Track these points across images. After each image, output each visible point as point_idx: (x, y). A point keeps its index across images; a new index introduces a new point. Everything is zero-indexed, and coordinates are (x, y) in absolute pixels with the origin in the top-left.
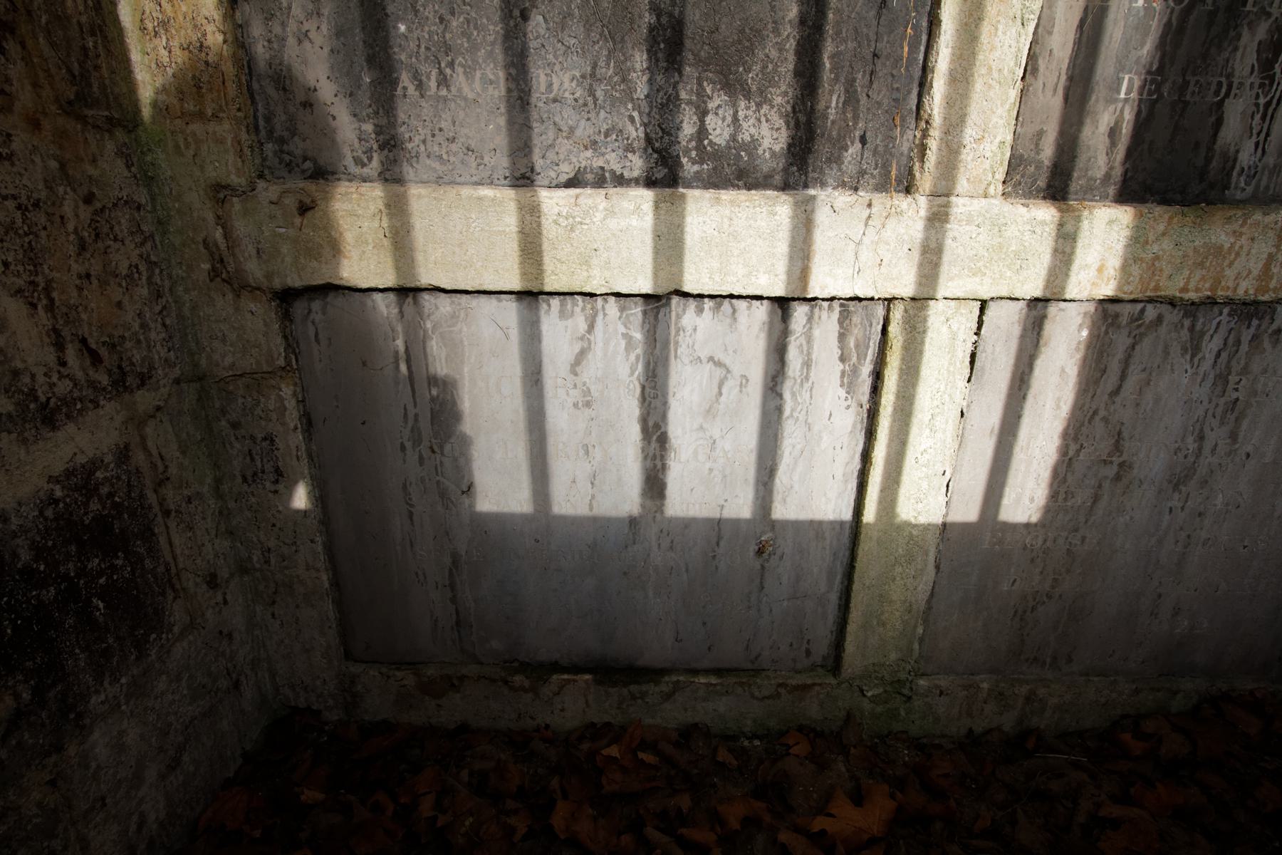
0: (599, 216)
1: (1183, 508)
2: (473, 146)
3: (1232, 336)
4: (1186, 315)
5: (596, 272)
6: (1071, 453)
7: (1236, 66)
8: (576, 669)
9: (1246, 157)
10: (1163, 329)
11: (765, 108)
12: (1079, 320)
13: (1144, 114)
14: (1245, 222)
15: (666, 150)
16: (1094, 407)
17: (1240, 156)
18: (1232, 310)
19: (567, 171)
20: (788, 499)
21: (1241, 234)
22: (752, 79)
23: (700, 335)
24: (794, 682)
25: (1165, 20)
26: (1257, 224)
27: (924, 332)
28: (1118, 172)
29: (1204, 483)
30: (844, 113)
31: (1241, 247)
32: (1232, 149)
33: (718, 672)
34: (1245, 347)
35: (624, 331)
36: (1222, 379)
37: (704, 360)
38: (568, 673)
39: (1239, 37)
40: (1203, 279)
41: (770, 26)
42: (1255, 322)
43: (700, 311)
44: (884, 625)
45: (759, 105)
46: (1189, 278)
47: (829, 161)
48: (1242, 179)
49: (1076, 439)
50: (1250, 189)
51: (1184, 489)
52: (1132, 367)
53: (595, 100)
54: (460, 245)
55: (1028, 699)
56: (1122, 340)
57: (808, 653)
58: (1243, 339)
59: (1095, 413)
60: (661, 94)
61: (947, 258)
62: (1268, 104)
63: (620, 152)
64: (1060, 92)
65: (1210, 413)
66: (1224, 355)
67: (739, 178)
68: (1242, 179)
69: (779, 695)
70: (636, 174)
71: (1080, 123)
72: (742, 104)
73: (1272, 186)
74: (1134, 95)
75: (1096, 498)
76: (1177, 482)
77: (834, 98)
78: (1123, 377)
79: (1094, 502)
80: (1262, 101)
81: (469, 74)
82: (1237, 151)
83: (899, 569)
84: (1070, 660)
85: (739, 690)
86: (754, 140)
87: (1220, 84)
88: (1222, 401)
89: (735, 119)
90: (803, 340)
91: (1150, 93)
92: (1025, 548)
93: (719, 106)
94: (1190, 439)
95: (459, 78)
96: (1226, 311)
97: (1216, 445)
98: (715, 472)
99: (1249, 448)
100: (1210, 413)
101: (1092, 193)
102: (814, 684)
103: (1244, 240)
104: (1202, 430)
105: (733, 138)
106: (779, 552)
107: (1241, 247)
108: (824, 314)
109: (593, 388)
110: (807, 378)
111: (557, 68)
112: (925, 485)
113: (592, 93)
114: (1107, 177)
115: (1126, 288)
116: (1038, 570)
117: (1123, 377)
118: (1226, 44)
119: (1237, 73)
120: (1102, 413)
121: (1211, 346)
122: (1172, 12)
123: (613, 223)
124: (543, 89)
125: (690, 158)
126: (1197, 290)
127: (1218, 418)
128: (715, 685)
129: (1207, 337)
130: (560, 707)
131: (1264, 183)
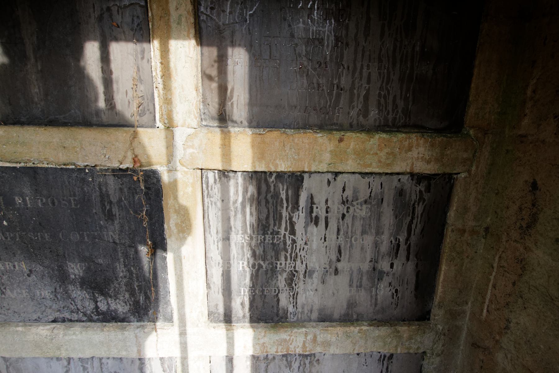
0: (61, 336)
2: (16, 311)
5: (63, 352)
9: (291, 309)
11: (118, 301)
13: (251, 298)
14: (292, 332)
17: (289, 309)
19: (51, 318)
22: (111, 292)
23: (110, 365)
27: (188, 366)
28: (248, 315)
32: (286, 308)
34: (308, 365)
39: (277, 277)
40: (282, 348)
45: (115, 300)
47: (144, 314)
48: (292, 315)
50: (295, 318)
53: (58, 298)
54: (12, 345)
62: (294, 295)
66: (301, 368)
68: (292, 315)
71: (230, 302)
72: (110, 299)
74: (247, 293)
77: (141, 297)
80: (291, 294)
81: (12, 291)
86: (115, 309)
87: (275, 290)
89: (108, 303)
91: (251, 293)
95: (8, 292)
103: (293, 337)
105: (108, 308)
111: (43, 289)
113: (56, 296)
114: (244, 316)
119: (280, 286)
123: (66, 338)
124: (39, 295)
126: (281, 352)
129: (293, 363)
131: (300, 316)
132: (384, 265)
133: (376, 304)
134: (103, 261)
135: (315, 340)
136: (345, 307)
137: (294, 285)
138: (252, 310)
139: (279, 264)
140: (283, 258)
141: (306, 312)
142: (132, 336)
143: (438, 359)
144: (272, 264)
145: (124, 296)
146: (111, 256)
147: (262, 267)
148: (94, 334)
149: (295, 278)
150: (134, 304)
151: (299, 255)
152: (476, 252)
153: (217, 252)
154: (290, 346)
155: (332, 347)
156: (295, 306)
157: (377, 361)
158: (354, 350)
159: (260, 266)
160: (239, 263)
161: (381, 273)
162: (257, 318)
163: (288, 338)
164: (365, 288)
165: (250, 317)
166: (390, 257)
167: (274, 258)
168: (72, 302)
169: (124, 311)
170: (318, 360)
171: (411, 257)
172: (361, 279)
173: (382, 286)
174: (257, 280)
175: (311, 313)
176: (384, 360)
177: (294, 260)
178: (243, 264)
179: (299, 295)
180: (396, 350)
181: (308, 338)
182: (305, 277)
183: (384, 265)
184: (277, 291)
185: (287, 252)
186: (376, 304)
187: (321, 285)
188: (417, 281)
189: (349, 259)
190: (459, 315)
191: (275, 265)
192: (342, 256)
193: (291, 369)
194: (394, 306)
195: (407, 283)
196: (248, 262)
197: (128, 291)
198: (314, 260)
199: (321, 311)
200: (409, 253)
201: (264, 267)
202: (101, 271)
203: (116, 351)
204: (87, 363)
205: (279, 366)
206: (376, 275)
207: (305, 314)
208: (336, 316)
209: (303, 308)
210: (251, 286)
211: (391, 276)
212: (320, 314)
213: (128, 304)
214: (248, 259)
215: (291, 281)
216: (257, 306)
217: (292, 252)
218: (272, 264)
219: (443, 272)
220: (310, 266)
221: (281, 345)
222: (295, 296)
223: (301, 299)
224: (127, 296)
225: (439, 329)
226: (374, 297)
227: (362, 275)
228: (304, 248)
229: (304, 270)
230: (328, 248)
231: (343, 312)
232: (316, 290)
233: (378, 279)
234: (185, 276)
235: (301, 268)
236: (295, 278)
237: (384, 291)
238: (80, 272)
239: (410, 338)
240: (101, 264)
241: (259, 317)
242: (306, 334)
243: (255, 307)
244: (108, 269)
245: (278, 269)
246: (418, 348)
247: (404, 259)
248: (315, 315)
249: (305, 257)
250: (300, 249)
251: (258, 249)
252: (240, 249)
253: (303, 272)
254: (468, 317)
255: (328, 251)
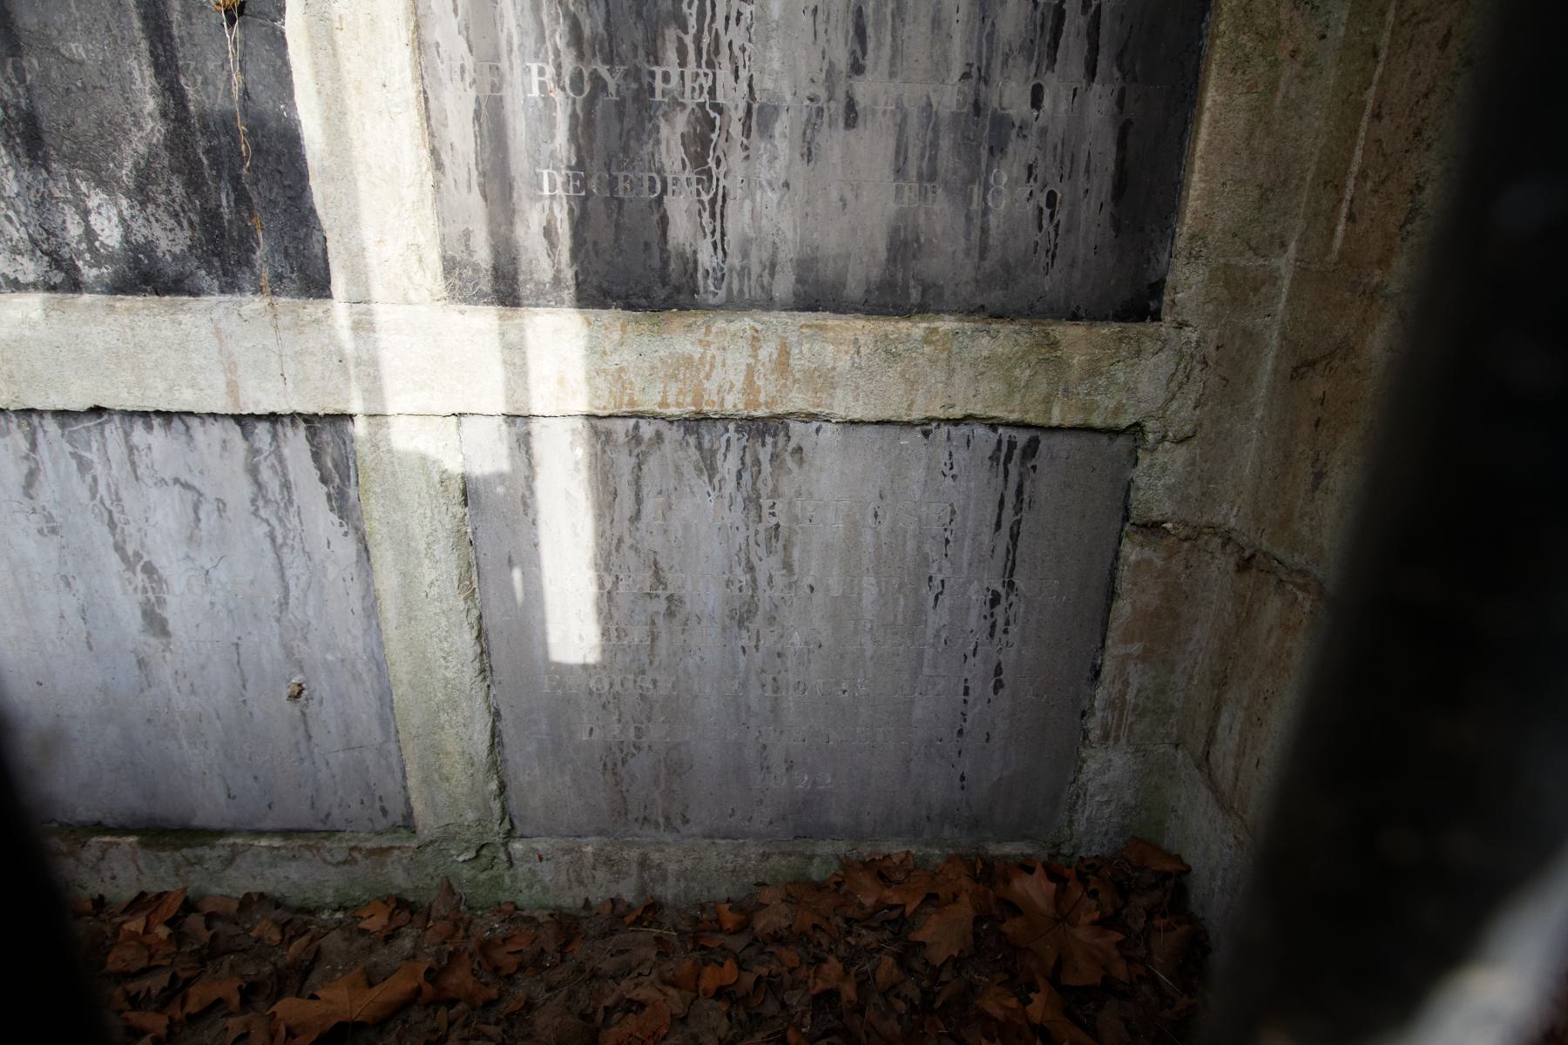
1: (756, 647)
3: (748, 455)
4: (687, 431)
6: (608, 586)
7: (664, 160)
8: (123, 831)
9: (706, 258)
10: (667, 447)
11: (151, 208)
12: (568, 437)
13: (577, 212)
15: (56, 252)
16: (617, 535)
17: (699, 256)
18: (738, 426)
20: (310, 637)
21: (708, 344)
23: (157, 454)
24: (369, 845)
25: (569, 110)
26: (723, 332)
28: (568, 274)
29: (772, 619)
30: (238, 212)
31: (713, 357)
32: (689, 251)
33: (287, 833)
34: (766, 468)
35: (71, 449)
36: (753, 501)
37: (171, 482)
38: (112, 835)
39: (657, 129)
40: (681, 392)
41: (129, 119)
42: (769, 440)
43: (150, 428)
44: (447, 779)
46: (665, 392)
48: (710, 281)
49: (608, 569)
50: (722, 293)
51: (751, 626)
52: (645, 491)
55: (644, 863)
56: (625, 462)
57: (384, 812)
58: (761, 457)
59: (620, 541)
60: (33, 192)
61: (386, 370)
62: (713, 201)
63: (7, 254)
64: (476, 189)
65: (752, 541)
66: (746, 476)
67: (146, 282)
68: (710, 281)
69: (354, 861)
70: (31, 278)
73: (746, 289)
74: (559, 191)
75: (654, 638)
76: (742, 616)
77: (223, 196)
78: (639, 500)
79: (653, 641)
80: (706, 198)
82: (695, 252)
83: (444, 717)
84: (686, 821)
85: (308, 854)
86: (149, 242)
87: (652, 179)
88: (761, 527)
90: (272, 459)
91: (577, 190)
92: (591, 693)
93: (100, 206)
94: (739, 571)
96: (732, 426)
97: (771, 577)
98: (218, 607)
99: (810, 580)
100: (752, 541)
101: (540, 298)
102: (392, 848)
103: (713, 350)
104: (748, 559)
106: (316, 695)
107: (713, 357)
108: (289, 431)
109: (54, 513)
110: (290, 501)
112: (444, 622)
114: (557, 281)
115: (597, 403)
116: (615, 718)
117: (639, 500)
118: (645, 137)
119: (667, 168)
120: (628, 541)
121: (728, 466)
122: (574, 102)
125: (86, 262)
126: (678, 405)
127: (763, 546)
128: (278, 848)
129: (720, 456)
130: (109, 874)
131: (735, 286)
132: (1011, 95)
133: (984, 250)
134: (87, 51)
135: (783, 364)
136: (882, 254)
137: (711, 163)
138: (581, 256)
139: (659, 77)
140: (672, 55)
141: (756, 269)
142: (203, 331)
143: (1182, 452)
144: (637, 79)
145: (168, 192)
146: (108, 29)
147: (605, 86)
148: (86, 322)
149: (714, 136)
150: (203, 223)
151: (724, 40)
152: (1323, 37)
153: (453, 23)
154: (707, 385)
155: (840, 393)
156: (719, 246)
157: (988, 463)
158: (910, 406)
159: (598, 84)
160: (527, 71)
161: (1001, 124)
162: (599, 287)
163: (697, 352)
164: (946, 183)
165: (578, 285)
166: (1030, 60)
167: (641, 52)
168: (11, 213)
169: (177, 250)
170: (799, 449)
171: (1103, 63)
172: (934, 145)
173: (1005, 179)
174: (591, 139)
175: (772, 275)
176: (1008, 458)
177: (710, 64)
178: (541, 72)
179: (730, 203)
180: (1048, 411)
181: (763, 354)
182: (747, 132)
183: (1011, 95)
184: (659, 186)
185: (686, 32)
186: (984, 250)
187: (800, 166)
188: (1121, 163)
189: (892, 63)
190: (1256, 290)
191: (646, 80)
192: (870, 54)
193: (716, 481)
194: (1044, 259)
195: (1087, 171)
196: (559, 67)
197: (178, 171)
198: (776, 65)
199: (806, 266)
200: (1094, 49)
201: (612, 88)
202: (84, 89)
203: (161, 386)
204: (88, 446)
205: (677, 468)
206: (983, 131)
207: (754, 277)
208: (854, 290)
209: (745, 255)
210: (573, 162)
211: (1033, 139)
212: (800, 280)
213: (185, 224)
214: (557, 53)
215: (700, 145)
216: (595, 243)
217: (700, 31)
218: (637, 79)
219: (1206, 117)
220: (765, 84)
221: (674, 377)
222: (717, 208)
223: (738, 220)
224: (178, 190)
225: (1188, 343)
226: (977, 222)
227: (936, 130)
228: (739, 14)
229: (742, 105)
230: (821, 16)
231: (875, 274)
232: (787, 185)
233: (991, 149)
234: (353, 102)
235: (732, 96)
236: (714, 136)
237: (1009, 197)
238: (17, 96)
239: (1093, 371)
240: (81, 63)
241: (605, 285)
242: (755, 341)
243: (589, 246)
244: (104, 82)
245: (658, 97)
246: (1118, 410)
247: (1077, 70)
248: (784, 285)
249: (743, 49)
250: (727, 18)
251: (591, 15)
252: (528, 12)
253: (741, 113)
254: (1284, 298)
255: (821, 29)
